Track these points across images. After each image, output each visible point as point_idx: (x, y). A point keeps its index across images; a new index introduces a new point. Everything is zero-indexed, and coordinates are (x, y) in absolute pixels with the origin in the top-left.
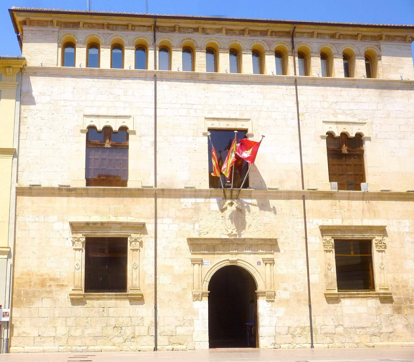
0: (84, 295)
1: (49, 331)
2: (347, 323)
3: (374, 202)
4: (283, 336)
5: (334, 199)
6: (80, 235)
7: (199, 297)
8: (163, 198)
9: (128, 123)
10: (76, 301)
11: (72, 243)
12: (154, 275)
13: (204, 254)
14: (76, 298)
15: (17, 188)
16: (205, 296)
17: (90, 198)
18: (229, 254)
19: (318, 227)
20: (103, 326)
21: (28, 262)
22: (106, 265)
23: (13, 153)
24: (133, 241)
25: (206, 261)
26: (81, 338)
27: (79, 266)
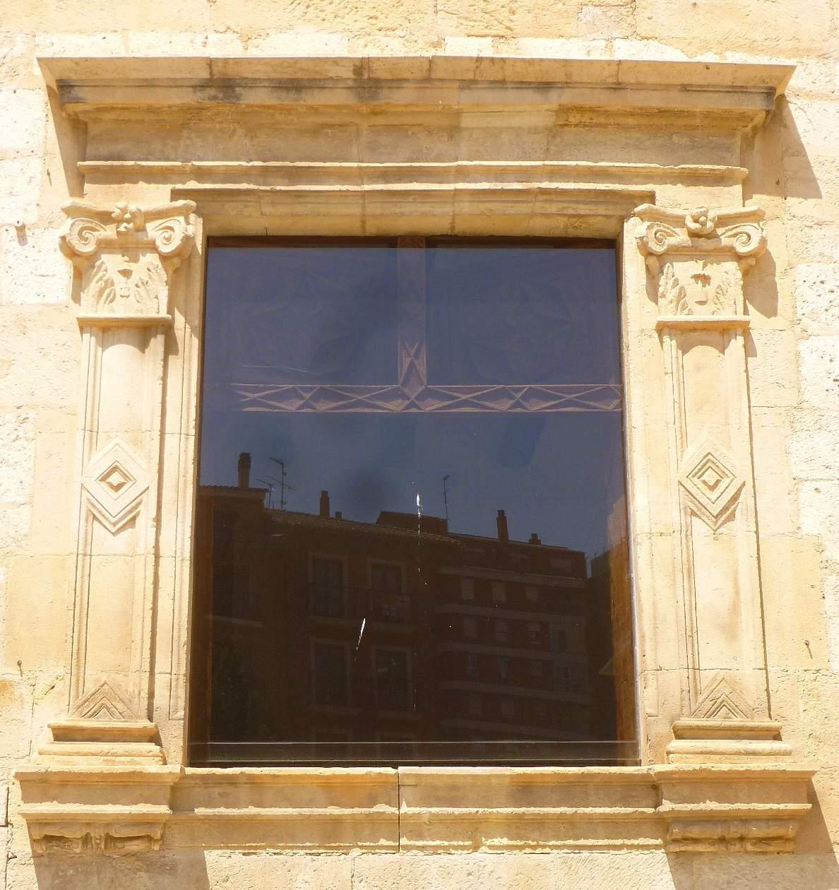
0: (177, 794)
6: (155, 196)
11: (63, 269)
14: (90, 822)
24: (677, 253)
27: (128, 494)
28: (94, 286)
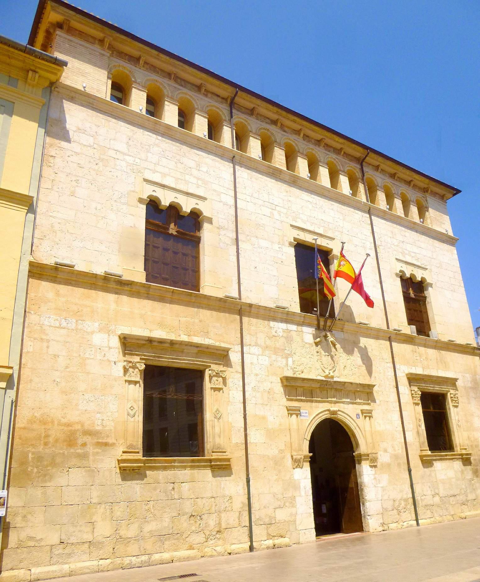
0: (144, 462)
1: (80, 531)
2: (442, 492)
3: (443, 352)
4: (390, 513)
5: (414, 345)
6: (136, 359)
7: (300, 462)
8: (249, 317)
9: (203, 207)
10: (129, 472)
12: (243, 430)
13: (301, 400)
14: (131, 467)
15: (31, 264)
16: (306, 461)
17: (150, 302)
18: (328, 402)
19: (404, 375)
20: (175, 514)
21: (42, 399)
22: (174, 411)
23: (28, 203)
25: (304, 411)
26: (138, 540)
27: (134, 411)
28: (128, 374)
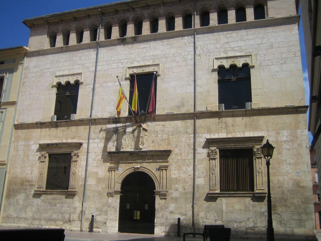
3: (255, 117)
